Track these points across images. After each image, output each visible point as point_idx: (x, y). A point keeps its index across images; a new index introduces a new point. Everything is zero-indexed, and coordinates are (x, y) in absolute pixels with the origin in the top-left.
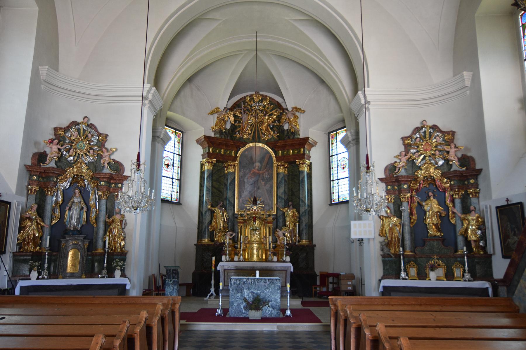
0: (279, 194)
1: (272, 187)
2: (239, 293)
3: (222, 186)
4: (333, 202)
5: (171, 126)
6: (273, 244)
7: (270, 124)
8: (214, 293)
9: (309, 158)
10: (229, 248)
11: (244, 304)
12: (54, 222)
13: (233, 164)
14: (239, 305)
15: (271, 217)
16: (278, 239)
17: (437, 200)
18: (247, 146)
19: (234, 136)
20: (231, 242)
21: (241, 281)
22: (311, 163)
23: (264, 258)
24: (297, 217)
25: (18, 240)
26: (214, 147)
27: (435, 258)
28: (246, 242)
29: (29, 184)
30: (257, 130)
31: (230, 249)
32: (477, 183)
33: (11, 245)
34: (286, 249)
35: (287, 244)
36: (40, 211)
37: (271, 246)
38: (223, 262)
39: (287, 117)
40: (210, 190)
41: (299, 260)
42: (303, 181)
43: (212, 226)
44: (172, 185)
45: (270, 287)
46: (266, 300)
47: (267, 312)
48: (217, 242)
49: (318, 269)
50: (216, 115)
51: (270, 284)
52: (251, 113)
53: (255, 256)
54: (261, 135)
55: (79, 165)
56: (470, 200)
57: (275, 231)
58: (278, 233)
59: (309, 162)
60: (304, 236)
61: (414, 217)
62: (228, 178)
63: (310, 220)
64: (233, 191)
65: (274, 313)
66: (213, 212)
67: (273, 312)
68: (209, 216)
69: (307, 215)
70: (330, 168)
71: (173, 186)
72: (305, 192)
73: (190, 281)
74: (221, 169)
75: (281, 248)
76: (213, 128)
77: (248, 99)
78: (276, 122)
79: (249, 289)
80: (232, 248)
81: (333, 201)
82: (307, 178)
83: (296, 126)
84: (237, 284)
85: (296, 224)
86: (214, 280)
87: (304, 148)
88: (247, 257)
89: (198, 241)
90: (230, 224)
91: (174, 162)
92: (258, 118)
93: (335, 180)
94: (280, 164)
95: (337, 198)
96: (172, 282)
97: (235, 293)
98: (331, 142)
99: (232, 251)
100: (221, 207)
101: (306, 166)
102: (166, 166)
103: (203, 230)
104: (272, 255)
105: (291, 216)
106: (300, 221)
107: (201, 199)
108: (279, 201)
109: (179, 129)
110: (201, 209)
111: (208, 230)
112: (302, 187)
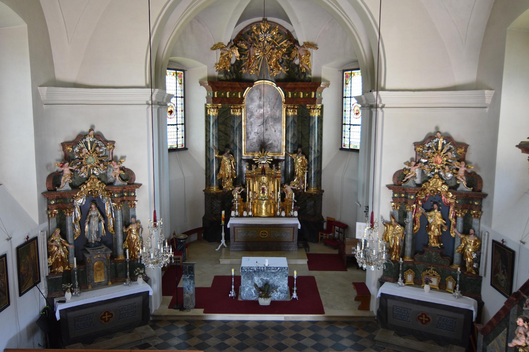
3: (228, 129)
5: (172, 68)
8: (225, 245)
10: (238, 203)
12: (75, 238)
14: (250, 290)
15: (280, 171)
17: (441, 213)
20: (240, 197)
23: (272, 212)
25: (48, 264)
27: (431, 269)
29: (48, 209)
32: (481, 205)
33: (44, 271)
36: (62, 225)
39: (298, 54)
41: (307, 207)
42: (313, 127)
49: (326, 213)
50: (219, 51)
53: (264, 211)
55: (91, 181)
56: (472, 219)
61: (417, 226)
63: (319, 166)
65: (282, 296)
66: (219, 160)
67: (281, 295)
70: (342, 110)
73: (201, 225)
74: (227, 110)
77: (255, 28)
81: (344, 146)
82: (318, 122)
83: (308, 66)
85: (305, 172)
87: (315, 91)
91: (177, 107)
93: (348, 97)
95: (348, 144)
96: (188, 277)
97: (246, 280)
98: (346, 81)
105: (300, 163)
110: (208, 156)
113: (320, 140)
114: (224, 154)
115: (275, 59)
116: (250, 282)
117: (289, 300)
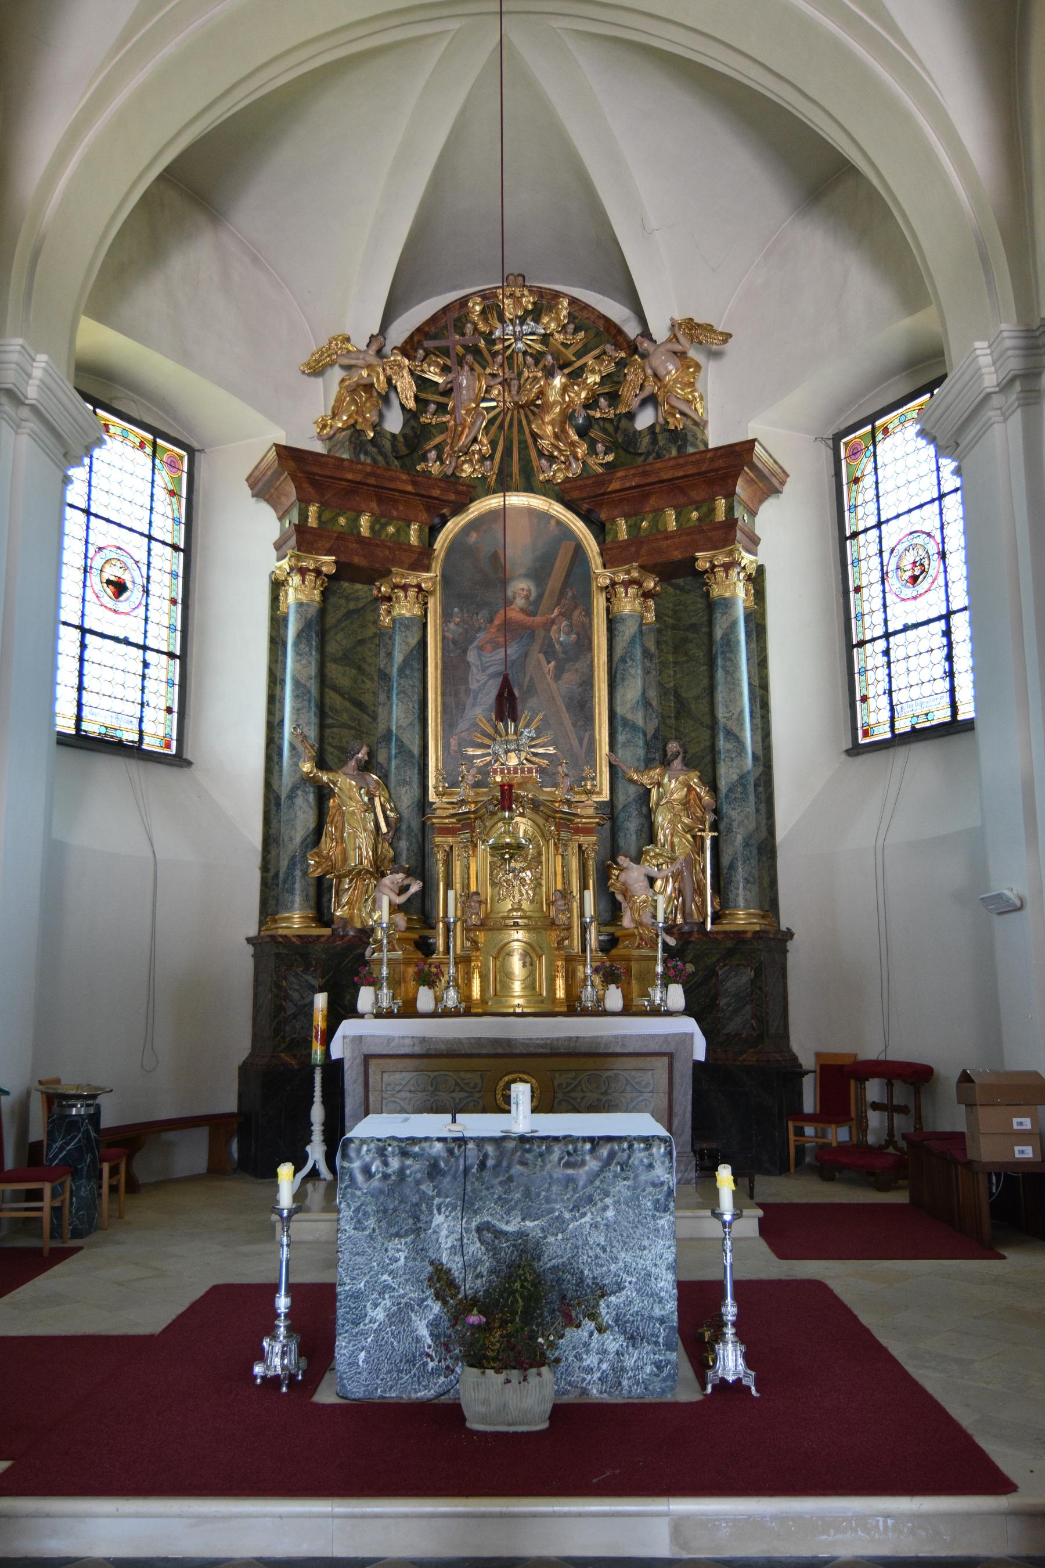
0: (620, 710)
1: (588, 683)
2: (397, 1235)
3: (368, 684)
4: (862, 741)
6: (599, 933)
7: (574, 411)
9: (753, 542)
10: (392, 949)
11: (436, 1307)
13: (414, 582)
14: (400, 1315)
16: (624, 905)
18: (478, 508)
19: (418, 468)
21: (415, 1156)
22: (761, 569)
23: (560, 993)
24: (704, 808)
26: (324, 506)
28: (474, 920)
30: (520, 442)
31: (399, 954)
34: (664, 951)
35: (669, 930)
37: (593, 938)
38: (362, 1016)
39: (649, 372)
40: (309, 692)
41: (723, 1002)
42: (730, 644)
43: (319, 855)
44: (144, 677)
45: (607, 1194)
46: (581, 1280)
47: (591, 1360)
48: (344, 927)
50: (337, 374)
51: (601, 1170)
52: (488, 371)
53: (517, 987)
54: (535, 463)
57: (610, 867)
58: (623, 877)
59: (752, 562)
60: (741, 893)
62: (393, 649)
63: (764, 822)
64: (416, 698)
66: (323, 794)
68: (308, 809)
69: (752, 798)
71: (146, 683)
72: (741, 694)
73: (229, 1104)
74: (363, 608)
75: (638, 947)
76: (324, 427)
77: (478, 308)
78: (602, 400)
79: (467, 1205)
80: (405, 950)
81: (866, 734)
82: (748, 635)
84: (386, 1177)
85: (702, 838)
86: (324, 1102)
87: (730, 495)
88: (476, 993)
89: (262, 923)
90: (403, 844)
91: (148, 578)
92: (520, 387)
94: (623, 577)
95: (886, 715)
97: (371, 1237)
99: (407, 962)
100: (366, 767)
101: (742, 575)
102: (110, 590)
103: (281, 876)
104: (597, 979)
106: (722, 826)
107: (276, 736)
108: (621, 738)
109: (173, 434)
111: (305, 873)
112: (727, 672)
113: (758, 712)
114: (344, 769)
115: (558, 410)
116: (400, 1251)
117: (688, 1393)
